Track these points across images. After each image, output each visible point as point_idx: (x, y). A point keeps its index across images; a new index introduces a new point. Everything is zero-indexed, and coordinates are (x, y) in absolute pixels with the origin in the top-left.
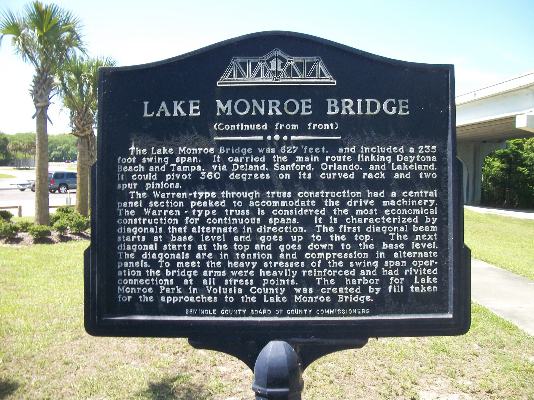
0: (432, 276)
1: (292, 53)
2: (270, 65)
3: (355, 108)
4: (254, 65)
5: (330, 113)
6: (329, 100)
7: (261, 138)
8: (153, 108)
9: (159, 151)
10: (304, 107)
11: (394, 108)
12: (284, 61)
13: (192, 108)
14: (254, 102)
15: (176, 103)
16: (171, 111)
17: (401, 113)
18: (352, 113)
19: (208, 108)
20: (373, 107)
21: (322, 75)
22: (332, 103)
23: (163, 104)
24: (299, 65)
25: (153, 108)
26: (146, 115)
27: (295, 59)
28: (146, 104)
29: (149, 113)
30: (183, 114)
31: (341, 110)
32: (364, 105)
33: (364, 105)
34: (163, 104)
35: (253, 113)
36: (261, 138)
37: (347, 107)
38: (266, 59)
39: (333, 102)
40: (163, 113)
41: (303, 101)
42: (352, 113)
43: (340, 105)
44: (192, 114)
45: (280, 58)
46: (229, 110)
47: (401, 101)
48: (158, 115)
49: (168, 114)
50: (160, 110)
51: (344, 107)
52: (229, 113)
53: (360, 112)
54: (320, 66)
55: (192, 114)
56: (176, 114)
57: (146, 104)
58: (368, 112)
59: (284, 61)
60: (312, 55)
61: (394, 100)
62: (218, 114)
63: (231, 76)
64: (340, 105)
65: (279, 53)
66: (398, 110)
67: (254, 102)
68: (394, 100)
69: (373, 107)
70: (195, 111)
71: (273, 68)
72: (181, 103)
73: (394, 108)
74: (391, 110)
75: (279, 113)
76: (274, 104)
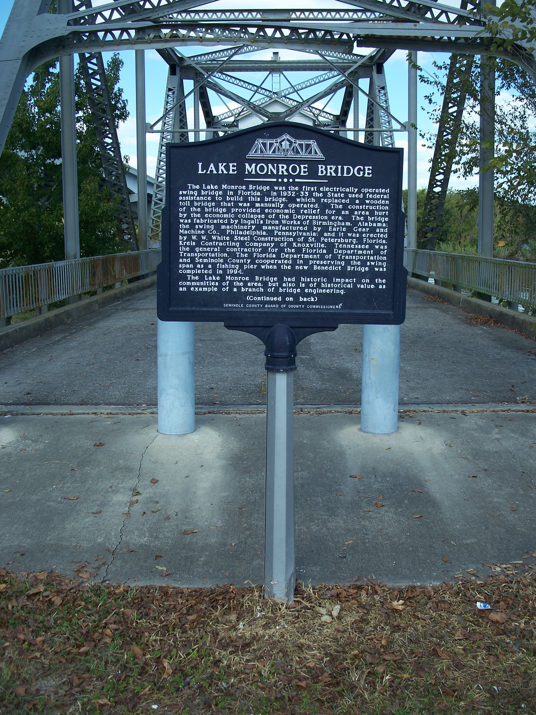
0: (384, 233)
1: (297, 137)
2: (281, 145)
3: (336, 171)
4: (271, 145)
5: (320, 174)
6: (320, 166)
7: (275, 180)
8: (205, 167)
9: (208, 187)
10: (303, 170)
11: (361, 173)
12: (291, 143)
13: (231, 168)
14: (270, 165)
15: (220, 164)
16: (217, 170)
17: (366, 175)
18: (334, 174)
19: (241, 168)
20: (349, 171)
21: (316, 153)
22: (321, 168)
23: (212, 165)
24: (301, 145)
25: (205, 167)
26: (200, 172)
27: (298, 142)
28: (200, 164)
29: (202, 171)
30: (225, 172)
31: (327, 173)
32: (342, 169)
33: (342, 169)
34: (212, 165)
35: (269, 173)
36: (275, 180)
37: (331, 170)
38: (279, 141)
39: (322, 167)
40: (212, 171)
41: (302, 166)
42: (334, 174)
43: (326, 169)
44: (231, 172)
45: (288, 140)
46: (254, 171)
47: (366, 168)
48: (209, 172)
49: (215, 172)
50: (210, 169)
51: (329, 170)
52: (254, 173)
53: (339, 175)
54: (314, 145)
55: (231, 172)
56: (220, 172)
57: (200, 164)
58: (345, 175)
59: (291, 143)
60: (309, 138)
61: (362, 167)
62: (247, 173)
63: (255, 152)
64: (326, 169)
65: (288, 137)
66: (364, 174)
67: (270, 165)
68: (362, 167)
69: (349, 171)
70: (233, 171)
71: (284, 147)
72: (224, 164)
73: (361, 173)
74: (359, 174)
75: (285, 173)
76: (283, 167)
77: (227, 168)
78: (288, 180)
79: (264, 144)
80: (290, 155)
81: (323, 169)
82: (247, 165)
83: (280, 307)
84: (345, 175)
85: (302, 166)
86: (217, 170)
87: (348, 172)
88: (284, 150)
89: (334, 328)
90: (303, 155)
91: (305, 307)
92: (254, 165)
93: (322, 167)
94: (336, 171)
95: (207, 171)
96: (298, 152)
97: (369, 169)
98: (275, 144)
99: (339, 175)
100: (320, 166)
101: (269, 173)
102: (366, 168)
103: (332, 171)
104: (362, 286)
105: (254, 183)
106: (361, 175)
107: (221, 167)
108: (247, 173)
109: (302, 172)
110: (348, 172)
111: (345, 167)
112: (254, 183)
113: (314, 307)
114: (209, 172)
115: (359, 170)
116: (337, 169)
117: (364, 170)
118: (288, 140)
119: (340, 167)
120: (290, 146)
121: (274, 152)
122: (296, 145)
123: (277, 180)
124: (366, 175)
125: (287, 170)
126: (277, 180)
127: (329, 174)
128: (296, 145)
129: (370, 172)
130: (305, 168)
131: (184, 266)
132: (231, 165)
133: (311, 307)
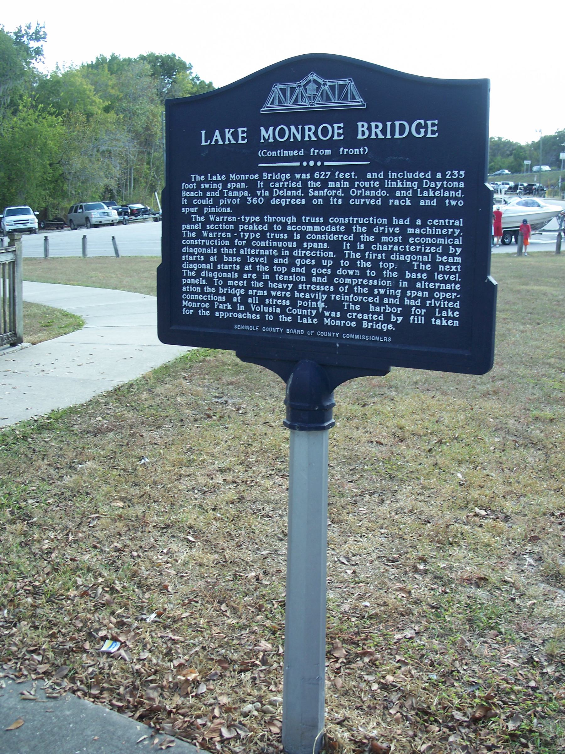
2: (306, 89)
3: (384, 131)
4: (293, 90)
5: (360, 137)
6: (360, 124)
7: (298, 164)
10: (336, 131)
11: (422, 130)
13: (240, 135)
15: (227, 131)
16: (223, 139)
18: (381, 136)
22: (362, 127)
23: (217, 133)
27: (329, 83)
28: (203, 132)
29: (206, 142)
30: (233, 142)
31: (370, 134)
32: (393, 127)
33: (393, 127)
34: (217, 133)
36: (298, 164)
38: (302, 84)
39: (363, 126)
40: (217, 141)
41: (336, 126)
42: (381, 136)
43: (369, 128)
44: (240, 141)
47: (429, 123)
48: (213, 143)
49: (221, 142)
50: (215, 138)
51: (374, 130)
53: (389, 136)
54: (351, 86)
55: (240, 141)
56: (227, 142)
57: (203, 132)
58: (397, 136)
61: (422, 122)
62: (262, 141)
63: (272, 103)
64: (369, 128)
65: (315, 77)
66: (426, 132)
67: (293, 128)
68: (422, 122)
71: (309, 93)
72: (232, 130)
73: (422, 130)
74: (419, 133)
77: (235, 135)
78: (315, 164)
79: (283, 91)
80: (319, 104)
81: (365, 129)
82: (262, 129)
83: (305, 333)
84: (397, 136)
85: (336, 126)
86: (223, 139)
87: (402, 132)
88: (309, 97)
89: (383, 372)
90: (335, 103)
91: (340, 336)
92: (271, 128)
93: (363, 126)
94: (384, 131)
95: (211, 142)
96: (328, 99)
97: (433, 125)
98: (298, 90)
99: (389, 136)
100: (360, 124)
101: (292, 140)
102: (429, 123)
103: (378, 131)
104: (397, 203)
105: (270, 170)
106: (422, 134)
107: (228, 135)
108: (262, 141)
109: (336, 135)
110: (402, 132)
111: (397, 123)
112: (270, 170)
113: (352, 336)
114: (213, 143)
115: (419, 127)
116: (385, 127)
117: (426, 127)
118: (315, 81)
119: (389, 124)
120: (318, 89)
121: (296, 101)
122: (326, 87)
123: (301, 164)
124: (429, 135)
125: (315, 134)
126: (301, 164)
127: (373, 136)
128: (326, 87)
129: (435, 128)
130: (339, 128)
131: (189, 242)
132: (240, 130)
133: (348, 336)
